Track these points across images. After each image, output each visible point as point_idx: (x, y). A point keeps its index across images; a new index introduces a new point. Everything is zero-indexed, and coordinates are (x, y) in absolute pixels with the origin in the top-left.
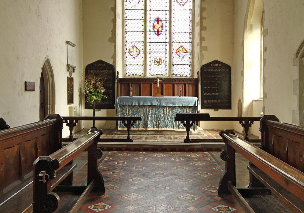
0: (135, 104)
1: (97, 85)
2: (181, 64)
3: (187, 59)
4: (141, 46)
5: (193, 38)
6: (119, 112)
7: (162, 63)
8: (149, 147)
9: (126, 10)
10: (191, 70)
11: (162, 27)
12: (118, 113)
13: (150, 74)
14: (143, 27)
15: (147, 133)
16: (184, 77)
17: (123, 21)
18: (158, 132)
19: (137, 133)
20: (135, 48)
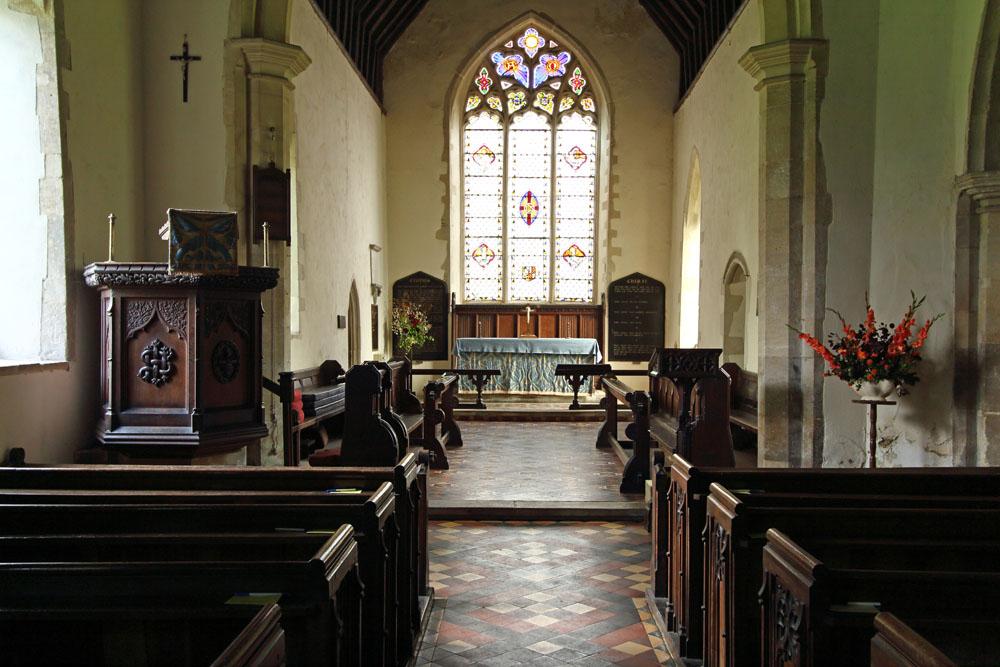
3: (585, 268)
11: (537, 208)
16: (578, 302)
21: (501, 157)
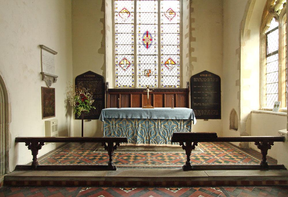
0: (122, 117)
1: (86, 96)
2: (170, 76)
3: (176, 71)
4: (131, 58)
5: (181, 51)
6: (104, 126)
7: (152, 75)
8: (137, 180)
9: (116, 24)
10: (179, 82)
11: (151, 40)
12: (103, 127)
13: (140, 85)
14: (133, 41)
15: (136, 149)
16: (173, 87)
17: (114, 34)
18: (148, 148)
19: (125, 149)
20: (125, 61)
21: (133, 14)
